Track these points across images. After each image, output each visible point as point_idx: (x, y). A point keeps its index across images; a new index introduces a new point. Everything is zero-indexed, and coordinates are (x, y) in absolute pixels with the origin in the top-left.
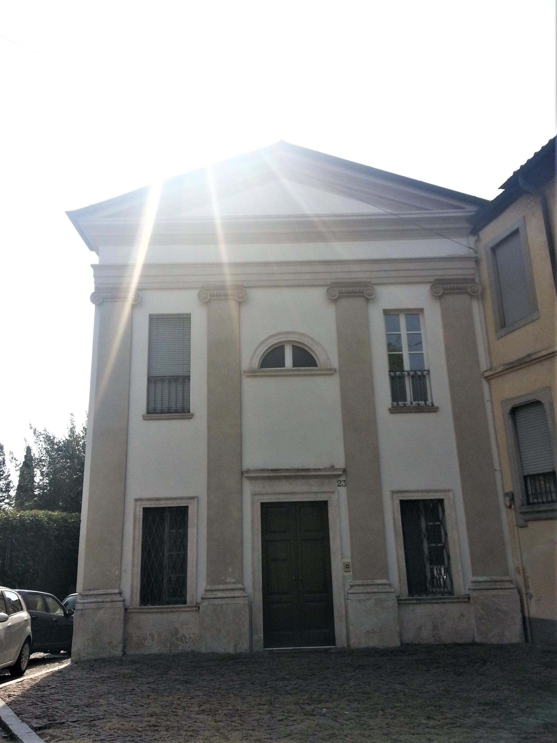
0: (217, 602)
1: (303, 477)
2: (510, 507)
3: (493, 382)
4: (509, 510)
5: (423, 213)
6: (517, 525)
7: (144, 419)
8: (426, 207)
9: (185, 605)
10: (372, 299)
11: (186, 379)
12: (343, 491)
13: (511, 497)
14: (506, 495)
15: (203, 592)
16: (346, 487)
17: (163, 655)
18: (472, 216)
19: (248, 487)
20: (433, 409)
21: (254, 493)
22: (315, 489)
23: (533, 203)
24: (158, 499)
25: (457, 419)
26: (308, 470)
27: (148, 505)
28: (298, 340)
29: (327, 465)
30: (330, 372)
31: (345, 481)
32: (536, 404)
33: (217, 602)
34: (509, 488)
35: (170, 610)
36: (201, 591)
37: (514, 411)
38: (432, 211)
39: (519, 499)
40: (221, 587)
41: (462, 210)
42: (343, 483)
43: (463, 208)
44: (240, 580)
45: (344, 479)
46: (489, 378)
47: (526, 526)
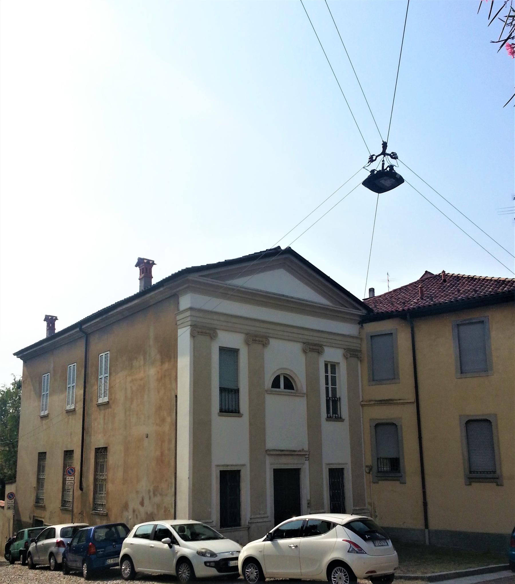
0: (259, 524)
1: (292, 455)
2: (369, 473)
3: (365, 408)
4: (368, 475)
5: (346, 309)
6: (372, 482)
7: (466, 485)
8: (346, 306)
9: (240, 527)
10: (322, 354)
11: (237, 391)
12: (307, 462)
13: (370, 468)
14: (367, 466)
15: (249, 519)
16: (308, 461)
17: (430, 572)
18: (363, 316)
19: (268, 460)
20: (339, 419)
21: (271, 463)
22: (296, 462)
23: (403, 324)
24: (228, 466)
25: (350, 426)
26: (294, 451)
27: (222, 469)
28: (288, 374)
29: (301, 449)
30: (301, 395)
31: (308, 458)
32: (393, 425)
33: (259, 524)
34: (369, 463)
35: (230, 530)
36: (248, 520)
37: (377, 426)
38: (349, 309)
39: (375, 469)
40: (258, 516)
41: (359, 311)
42: (307, 459)
43: (360, 310)
44: (265, 513)
45: (308, 457)
46: (363, 405)
47: (377, 483)
